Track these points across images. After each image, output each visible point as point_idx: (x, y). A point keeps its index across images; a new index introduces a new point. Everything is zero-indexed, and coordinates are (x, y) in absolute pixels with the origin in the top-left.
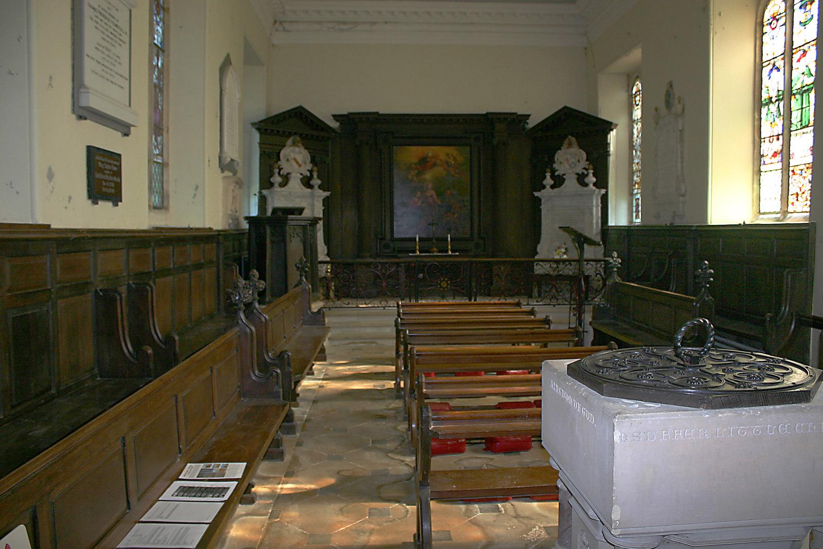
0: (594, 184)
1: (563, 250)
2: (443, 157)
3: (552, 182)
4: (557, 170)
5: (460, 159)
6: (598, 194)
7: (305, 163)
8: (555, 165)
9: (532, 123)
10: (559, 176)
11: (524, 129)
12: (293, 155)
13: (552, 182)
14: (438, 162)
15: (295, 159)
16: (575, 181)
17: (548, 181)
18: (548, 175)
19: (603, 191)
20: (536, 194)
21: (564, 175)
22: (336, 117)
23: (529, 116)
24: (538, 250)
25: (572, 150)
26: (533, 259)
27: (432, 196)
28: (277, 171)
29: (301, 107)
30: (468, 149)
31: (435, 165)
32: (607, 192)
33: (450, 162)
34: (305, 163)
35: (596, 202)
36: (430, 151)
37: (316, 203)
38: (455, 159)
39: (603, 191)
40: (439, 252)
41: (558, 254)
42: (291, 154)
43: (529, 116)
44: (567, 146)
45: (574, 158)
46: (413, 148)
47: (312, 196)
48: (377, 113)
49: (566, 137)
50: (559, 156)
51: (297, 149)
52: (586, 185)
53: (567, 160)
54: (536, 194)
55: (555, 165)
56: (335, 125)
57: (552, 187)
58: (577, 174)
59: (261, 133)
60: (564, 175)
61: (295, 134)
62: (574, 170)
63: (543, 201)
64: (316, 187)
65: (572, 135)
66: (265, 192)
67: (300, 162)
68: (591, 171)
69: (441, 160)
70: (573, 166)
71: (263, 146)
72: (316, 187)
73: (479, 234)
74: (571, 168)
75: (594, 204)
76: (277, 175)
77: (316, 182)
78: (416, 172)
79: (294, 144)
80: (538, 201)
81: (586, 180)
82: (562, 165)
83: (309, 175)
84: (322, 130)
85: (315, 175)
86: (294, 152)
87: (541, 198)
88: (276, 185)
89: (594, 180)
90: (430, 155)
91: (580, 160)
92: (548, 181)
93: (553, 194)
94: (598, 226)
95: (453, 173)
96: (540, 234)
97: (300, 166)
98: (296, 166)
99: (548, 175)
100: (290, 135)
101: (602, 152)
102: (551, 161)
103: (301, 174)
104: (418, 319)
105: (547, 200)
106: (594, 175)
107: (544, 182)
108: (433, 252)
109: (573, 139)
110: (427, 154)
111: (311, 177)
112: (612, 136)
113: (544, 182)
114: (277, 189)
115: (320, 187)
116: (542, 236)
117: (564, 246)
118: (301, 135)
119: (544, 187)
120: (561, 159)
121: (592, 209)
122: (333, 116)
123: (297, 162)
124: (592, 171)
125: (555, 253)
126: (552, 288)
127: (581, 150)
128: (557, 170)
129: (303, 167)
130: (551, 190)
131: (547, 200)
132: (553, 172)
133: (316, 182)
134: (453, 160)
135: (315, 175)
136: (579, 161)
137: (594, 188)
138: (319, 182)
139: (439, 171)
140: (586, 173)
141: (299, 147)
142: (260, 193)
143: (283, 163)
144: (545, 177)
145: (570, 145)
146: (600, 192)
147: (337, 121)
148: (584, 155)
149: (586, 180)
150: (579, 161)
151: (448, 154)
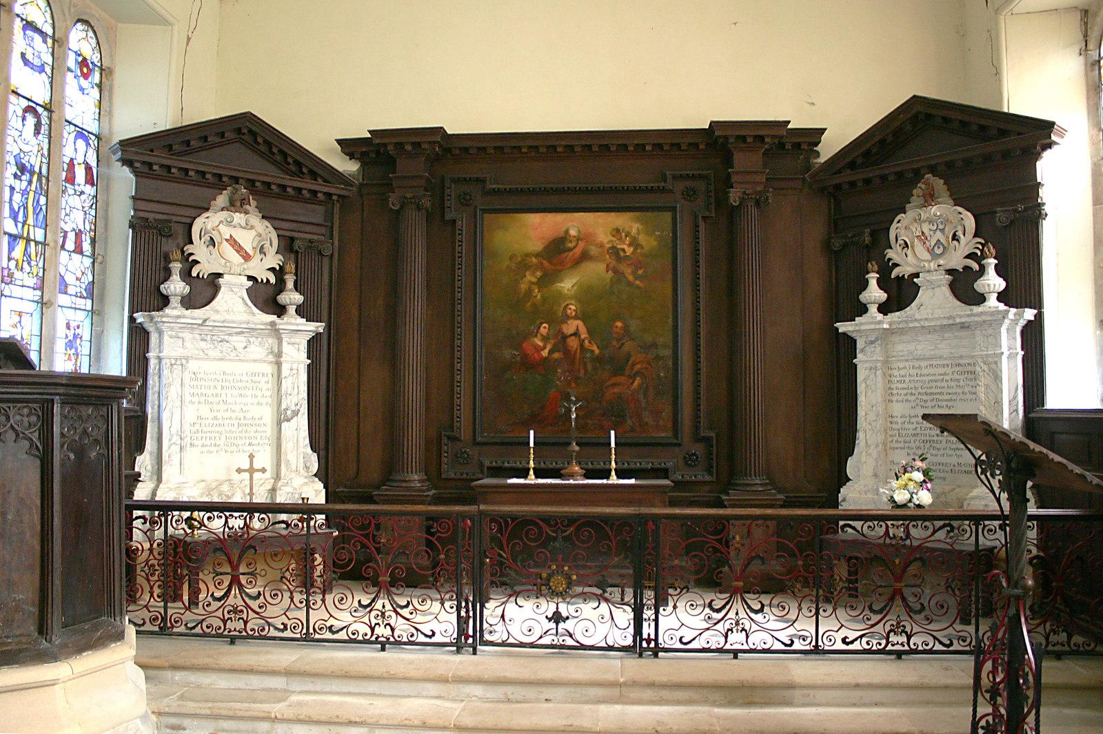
0: (1002, 297)
1: (918, 476)
2: (604, 237)
3: (882, 296)
4: (896, 265)
5: (648, 242)
6: (1015, 322)
7: (262, 251)
8: (890, 254)
9: (828, 148)
10: (900, 279)
11: (808, 167)
12: (226, 231)
13: (882, 296)
14: (594, 250)
15: (233, 242)
16: (946, 291)
17: (874, 293)
18: (873, 278)
19: (1029, 314)
20: (843, 327)
21: (917, 275)
22: (349, 146)
23: (823, 131)
24: (850, 471)
25: (935, 210)
26: (831, 512)
27: (576, 334)
28: (176, 267)
29: (248, 117)
30: (667, 216)
31: (585, 257)
32: (1039, 317)
33: (623, 250)
34: (262, 251)
35: (1010, 345)
36: (573, 223)
37: (286, 348)
38: (634, 243)
39: (1029, 314)
40: (587, 476)
41: (905, 487)
42: (222, 228)
43: (823, 131)
44: (921, 200)
45: (942, 231)
46: (534, 219)
47: (276, 332)
48: (440, 130)
49: (917, 175)
50: (903, 227)
51: (238, 218)
52: (981, 299)
53: (923, 238)
54: (843, 327)
55: (890, 254)
56: (347, 166)
57: (884, 309)
58: (950, 272)
59: (137, 173)
60: (917, 275)
61: (236, 180)
62: (941, 262)
63: (860, 345)
64: (292, 310)
65: (933, 170)
66: (140, 317)
67: (248, 249)
68: (992, 262)
69: (602, 246)
70: (938, 251)
71: (142, 205)
72: (292, 310)
73: (696, 427)
74: (935, 256)
75: (1004, 348)
76: (176, 277)
77: (291, 297)
78: (539, 274)
79: (235, 205)
80: (849, 343)
81: (980, 285)
82: (909, 252)
83: (273, 280)
84: (314, 175)
85: (290, 284)
86: (229, 223)
87: (853, 335)
88: (175, 301)
89: (1001, 284)
90: (573, 232)
91: (960, 234)
92: (874, 293)
93: (886, 326)
94: (1016, 411)
95: (631, 278)
96: (775, 122)
97: (247, 257)
98: (236, 258)
99: (873, 278)
100: (219, 183)
101: (1021, 207)
102: (880, 239)
103: (250, 278)
104: (1021, 298)
105: (872, 342)
106: (1000, 271)
107: (864, 297)
108: (571, 476)
109: (939, 183)
110: (567, 232)
111: (280, 286)
112: (1048, 167)
113: (864, 297)
114: (174, 310)
115: (300, 311)
116: (860, 435)
117: (919, 464)
118: (251, 184)
119: (863, 309)
120: (904, 237)
121: (997, 364)
122: (339, 142)
123: (239, 249)
124: (993, 261)
125: (895, 484)
126: (892, 599)
127: (960, 209)
128: (896, 265)
129: (255, 262)
130: (880, 316)
131: (872, 342)
132: (886, 269)
133: (291, 297)
134: (630, 245)
135: (290, 284)
136: (955, 238)
137: (1002, 306)
138: (298, 298)
139: (596, 271)
140: (976, 267)
141: (246, 213)
142: (132, 320)
143: (198, 249)
144: (864, 285)
145: (930, 198)
146: (1021, 315)
147: (352, 156)
148: (970, 221)
149: (980, 285)
150: (955, 238)
151: (618, 230)
